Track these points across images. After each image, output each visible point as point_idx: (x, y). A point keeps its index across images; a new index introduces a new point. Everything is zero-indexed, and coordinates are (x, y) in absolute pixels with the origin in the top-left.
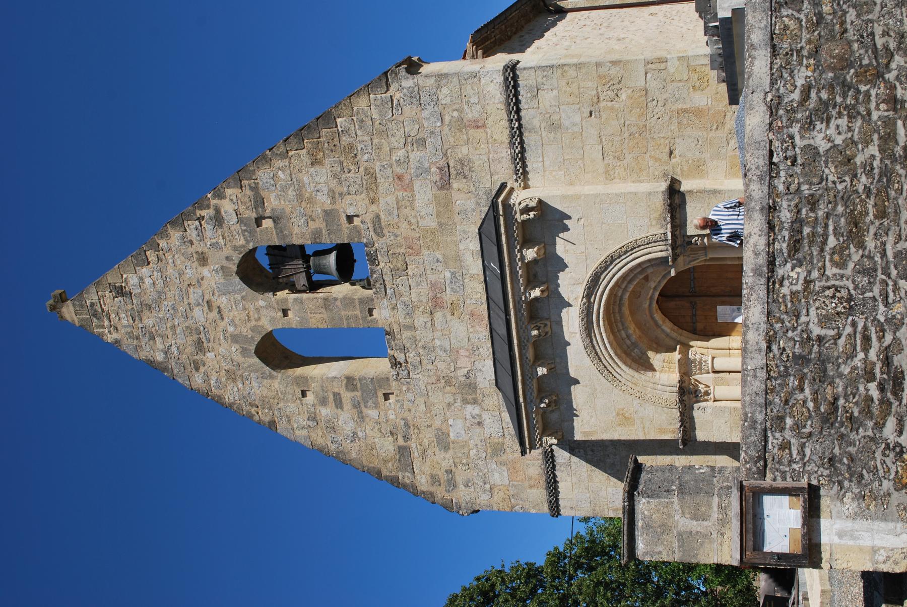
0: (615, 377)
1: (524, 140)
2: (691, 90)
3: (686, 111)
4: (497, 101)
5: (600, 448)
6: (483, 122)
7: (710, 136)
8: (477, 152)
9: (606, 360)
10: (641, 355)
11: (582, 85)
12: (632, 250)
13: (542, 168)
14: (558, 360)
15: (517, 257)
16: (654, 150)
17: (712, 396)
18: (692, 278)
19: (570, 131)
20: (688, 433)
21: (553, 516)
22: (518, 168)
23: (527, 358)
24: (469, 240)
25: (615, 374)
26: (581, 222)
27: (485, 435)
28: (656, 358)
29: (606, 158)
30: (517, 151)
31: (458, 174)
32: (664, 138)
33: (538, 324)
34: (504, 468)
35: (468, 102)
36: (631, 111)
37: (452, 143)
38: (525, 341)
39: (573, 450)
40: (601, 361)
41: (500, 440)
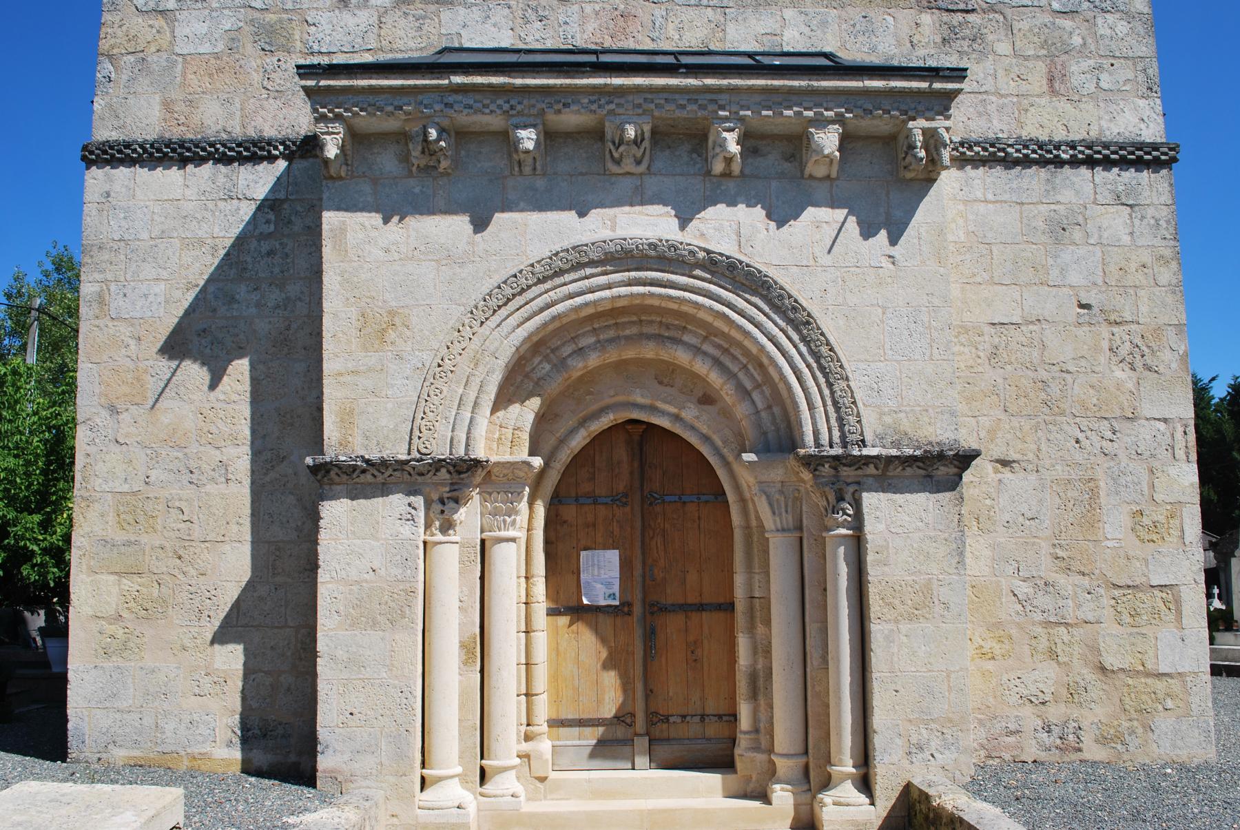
0: (495, 311)
1: (1030, 167)
2: (1135, 508)
3: (1094, 494)
4: (1103, 123)
5: (276, 270)
6: (1062, 92)
7: (1043, 544)
8: (1001, 73)
9: (540, 295)
10: (535, 376)
11: (1142, 293)
12: (822, 369)
13: (972, 196)
14: (540, 183)
15: (826, 110)
16: (1012, 428)
17: (439, 537)
18: (684, 498)
19: (1050, 261)
20: (345, 477)
21: (85, 148)
22: (976, 149)
23: (566, 105)
24: (806, 30)
25: (503, 312)
26: (886, 263)
27: (313, 13)
28: (524, 414)
29: (993, 331)
30: (1010, 150)
32: (1039, 450)
33: (646, 144)
34: (220, 47)
35: (1100, 68)
36: (1092, 387)
37: (1016, 25)
38: (612, 106)
39: (272, 208)
40: (540, 281)
41: (298, 45)
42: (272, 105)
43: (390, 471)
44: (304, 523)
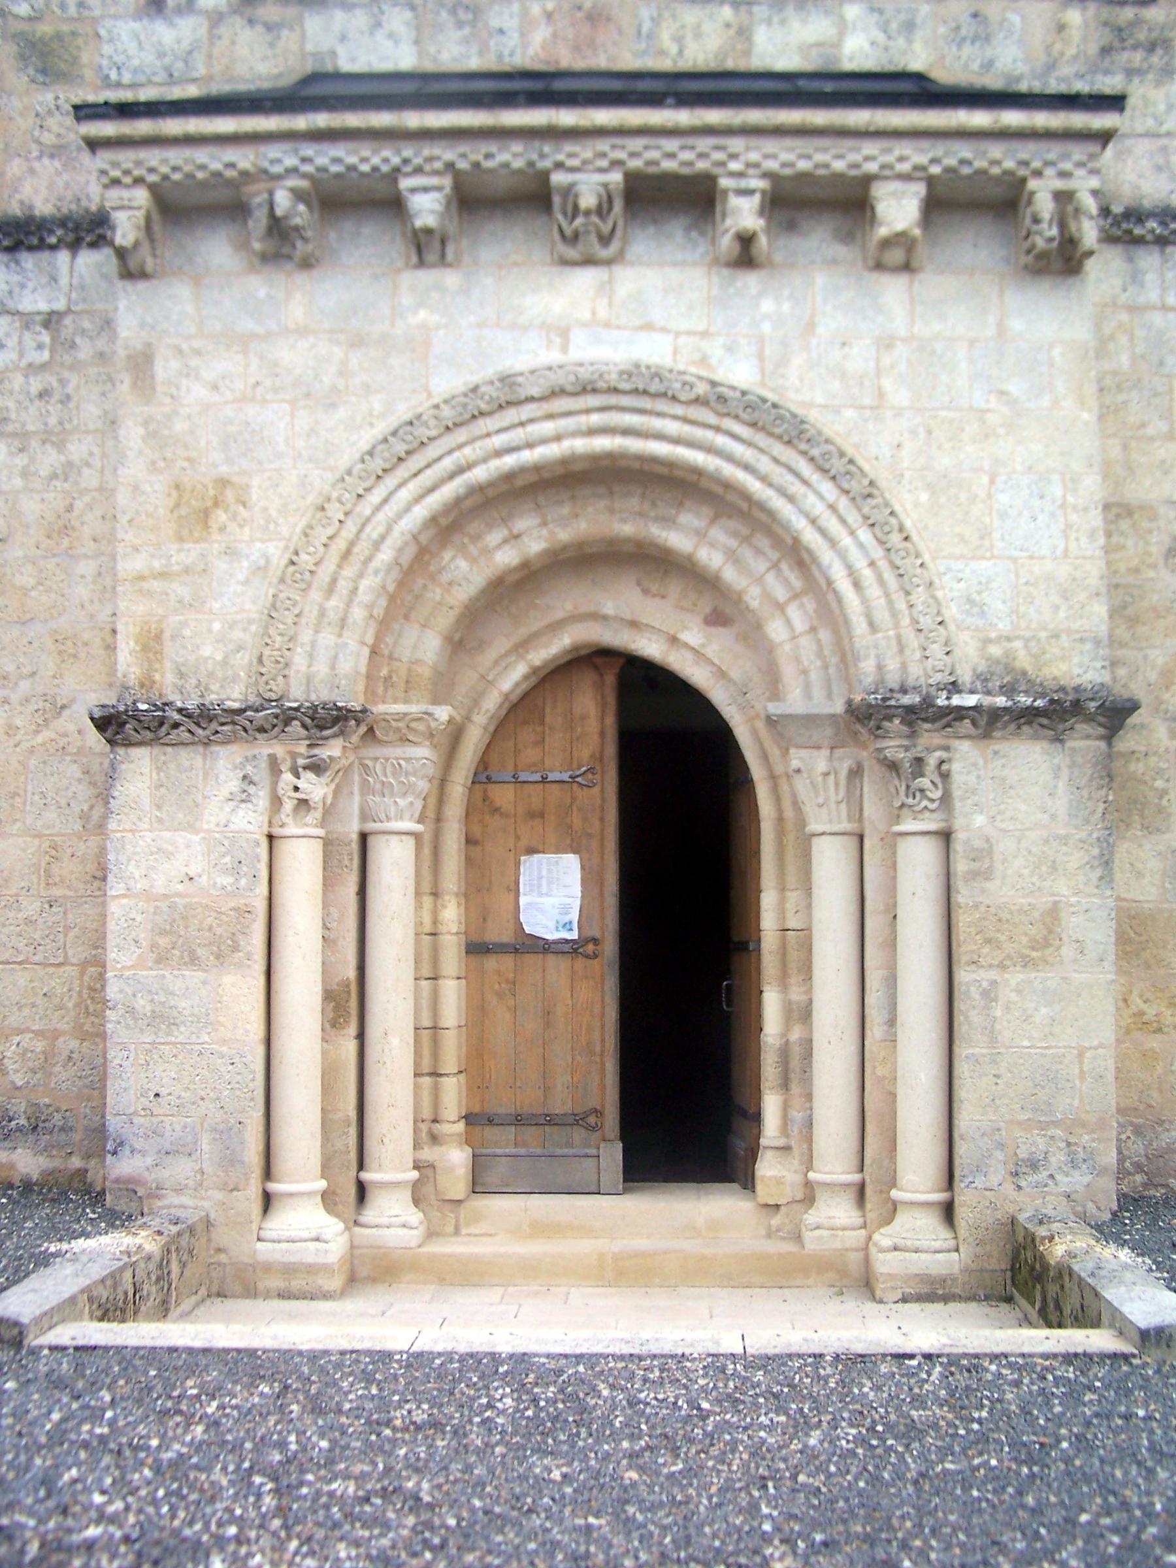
5: (53, 421)
9: (450, 452)
24: (881, 37)
25: (390, 482)
31: (1120, 32)
42: (48, 166)
43: (214, 726)
44: (92, 807)
